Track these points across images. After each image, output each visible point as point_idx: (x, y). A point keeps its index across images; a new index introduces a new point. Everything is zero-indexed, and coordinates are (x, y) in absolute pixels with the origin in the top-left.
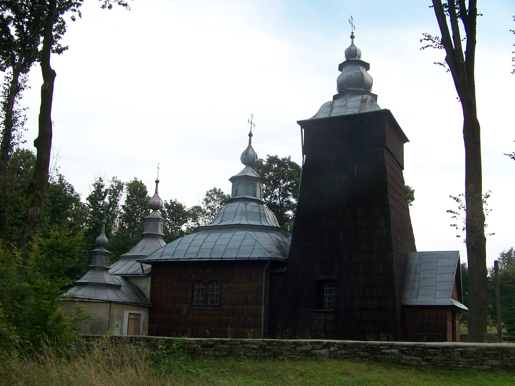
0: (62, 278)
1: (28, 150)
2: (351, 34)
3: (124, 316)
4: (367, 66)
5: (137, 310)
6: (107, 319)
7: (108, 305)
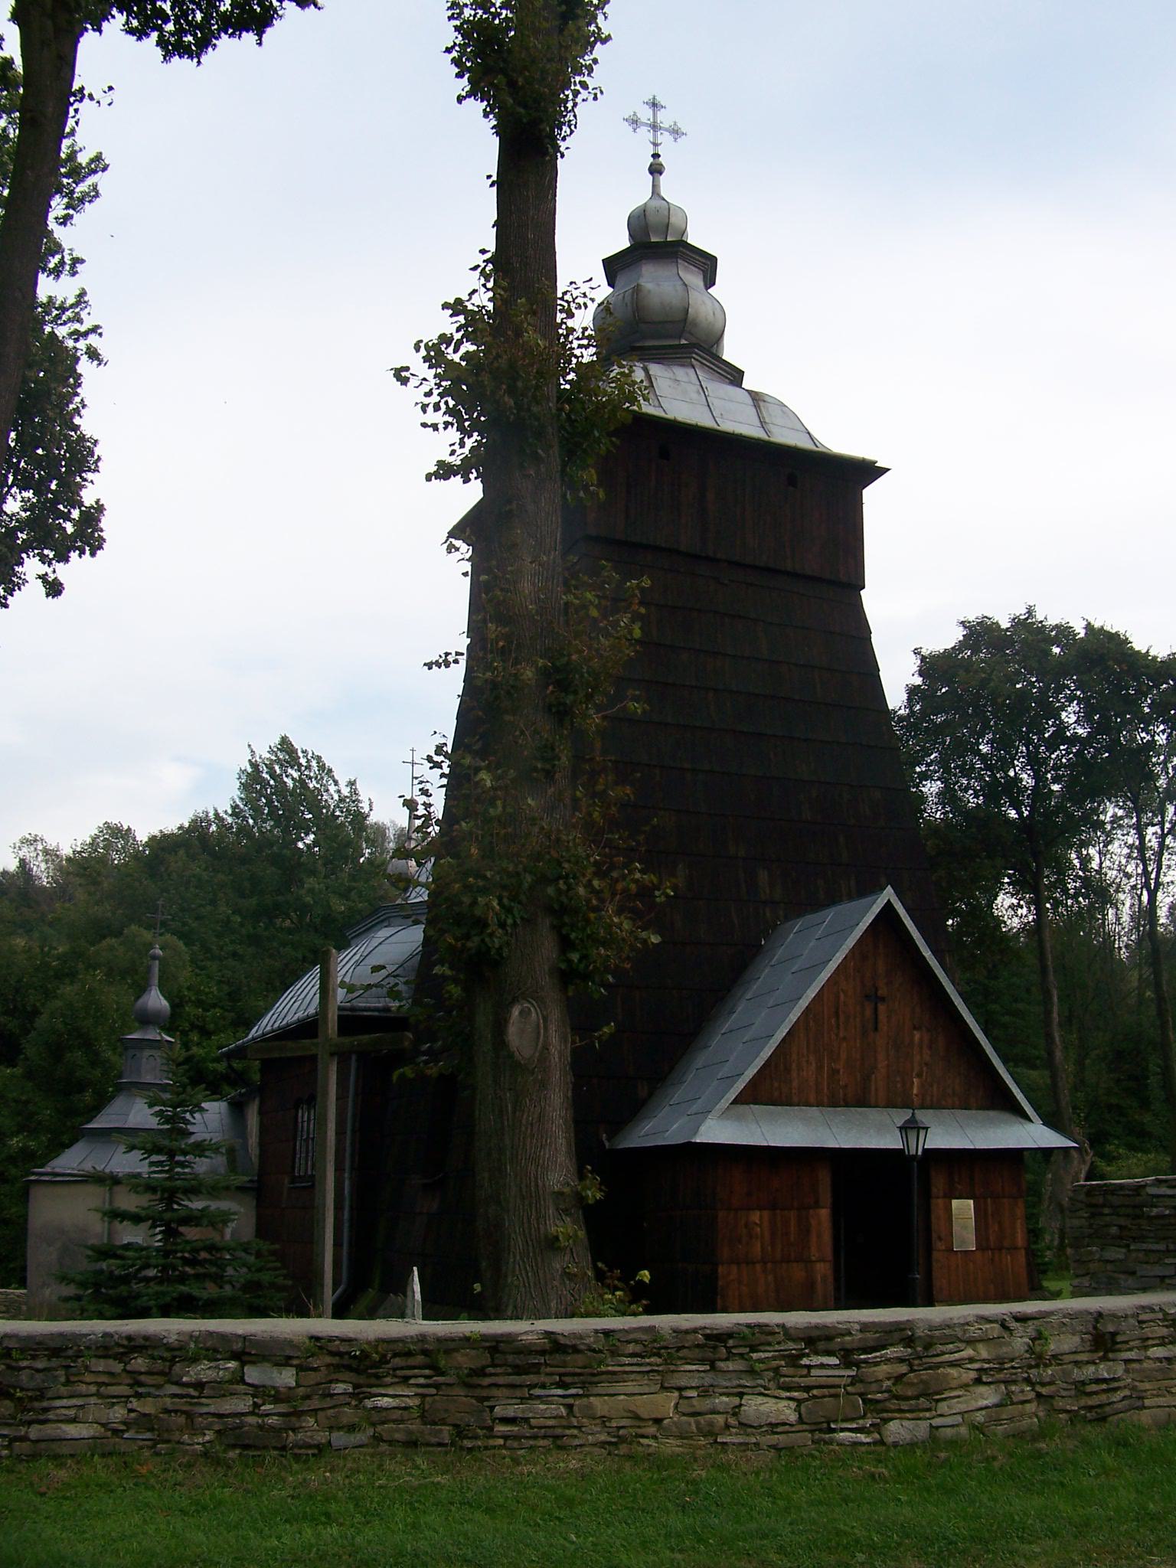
0: (239, 920)
1: (93, 554)
2: (652, 160)
4: (707, 265)
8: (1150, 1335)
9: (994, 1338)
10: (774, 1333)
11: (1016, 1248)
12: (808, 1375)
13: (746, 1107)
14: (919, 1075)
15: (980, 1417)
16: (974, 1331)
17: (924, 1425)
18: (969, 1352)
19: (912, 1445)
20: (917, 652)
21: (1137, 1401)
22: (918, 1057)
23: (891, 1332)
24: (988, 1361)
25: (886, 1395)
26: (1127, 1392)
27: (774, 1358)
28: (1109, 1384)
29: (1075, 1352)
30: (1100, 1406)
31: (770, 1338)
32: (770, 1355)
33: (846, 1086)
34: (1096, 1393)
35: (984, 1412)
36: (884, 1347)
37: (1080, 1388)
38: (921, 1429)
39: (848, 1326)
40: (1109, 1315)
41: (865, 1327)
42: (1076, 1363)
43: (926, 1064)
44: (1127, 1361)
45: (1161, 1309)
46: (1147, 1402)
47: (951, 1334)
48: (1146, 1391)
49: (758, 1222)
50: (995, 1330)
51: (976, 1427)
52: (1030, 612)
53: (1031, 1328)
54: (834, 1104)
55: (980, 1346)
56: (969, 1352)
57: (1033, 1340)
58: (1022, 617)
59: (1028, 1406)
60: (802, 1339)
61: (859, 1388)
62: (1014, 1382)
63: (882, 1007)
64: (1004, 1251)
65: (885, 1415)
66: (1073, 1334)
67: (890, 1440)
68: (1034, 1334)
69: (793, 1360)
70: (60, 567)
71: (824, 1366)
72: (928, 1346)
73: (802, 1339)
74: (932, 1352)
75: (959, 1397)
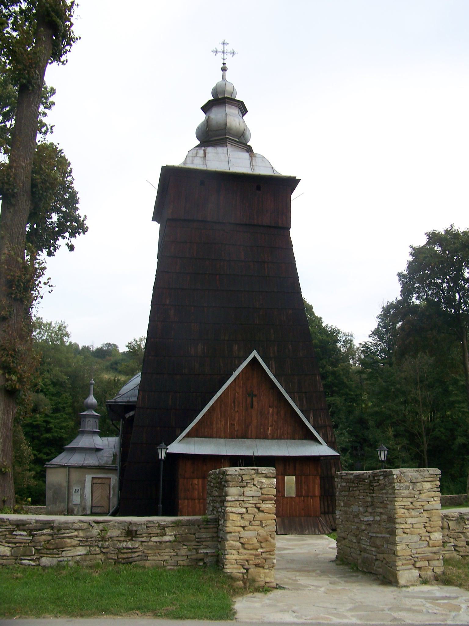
1: (84, 233)
3: (85, 480)
5: (104, 473)
6: (65, 484)
7: (66, 470)
8: (151, 532)
9: (84, 529)
10: (5, 522)
11: (315, 496)
12: (15, 538)
13: (193, 438)
14: (271, 426)
15: (78, 558)
16: (76, 526)
17: (56, 560)
18: (76, 533)
19: (51, 567)
20: (411, 247)
21: (145, 557)
22: (271, 419)
23: (45, 524)
24: (83, 538)
25: (42, 547)
26: (140, 554)
27: (5, 531)
28: (133, 550)
29: (118, 537)
30: (127, 558)
31: (4, 524)
32: (4, 530)
33: (238, 430)
34: (126, 553)
35: (80, 557)
36: (43, 529)
37: (119, 550)
38: (55, 561)
39: (31, 521)
40: (134, 524)
41: (37, 521)
42: (120, 541)
43: (275, 421)
44: (142, 542)
45: (158, 523)
46: (149, 558)
47: (67, 526)
48: (148, 554)
49: (197, 483)
50: (85, 526)
51: (77, 562)
52: (452, 227)
53: (101, 526)
54: (232, 437)
55: (80, 532)
56: (76, 533)
57: (101, 531)
58: (449, 229)
59: (98, 556)
60: (15, 525)
61: (33, 544)
62: (92, 546)
63: (255, 399)
64: (309, 498)
65: (41, 555)
66: (119, 530)
67: (43, 564)
68: (102, 528)
69: (11, 532)
70: (73, 239)
71: (22, 535)
72: (59, 530)
73: (15, 525)
74: (61, 532)
75: (70, 550)
